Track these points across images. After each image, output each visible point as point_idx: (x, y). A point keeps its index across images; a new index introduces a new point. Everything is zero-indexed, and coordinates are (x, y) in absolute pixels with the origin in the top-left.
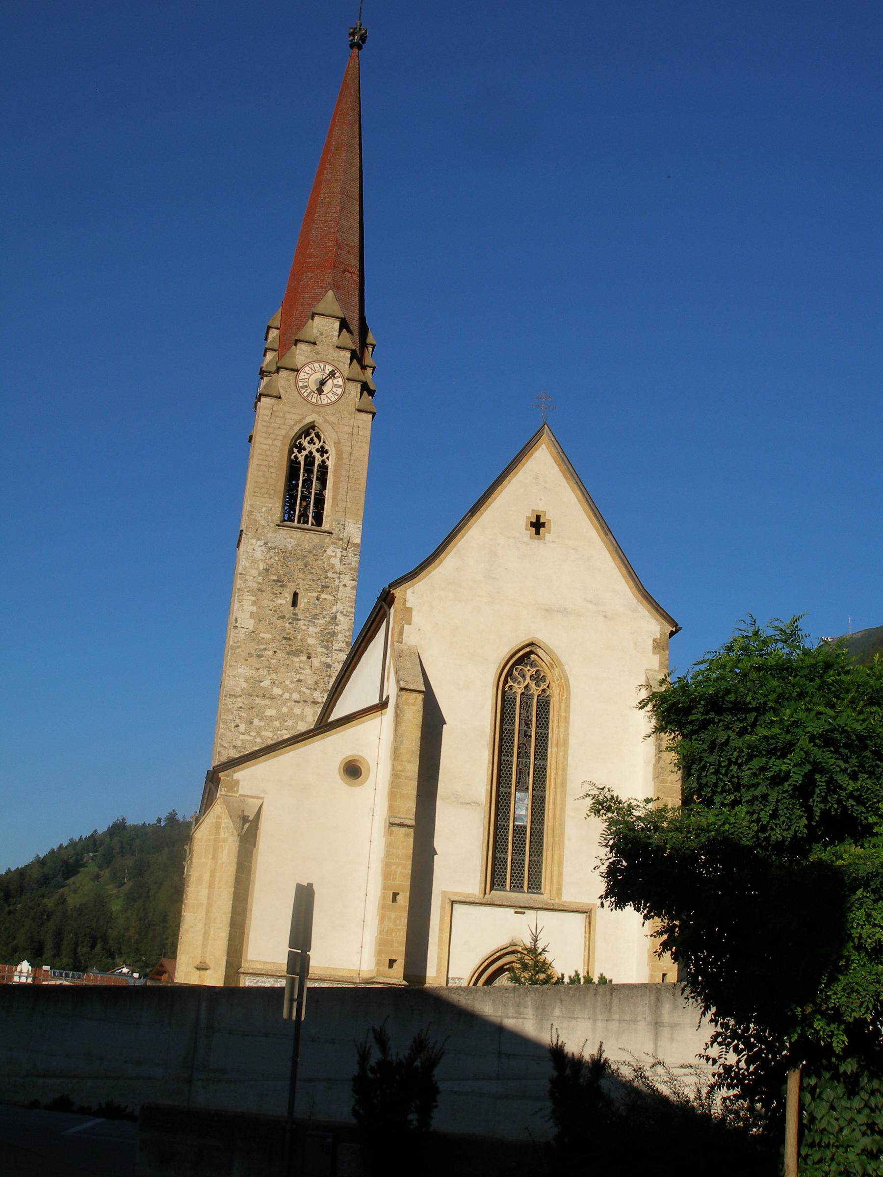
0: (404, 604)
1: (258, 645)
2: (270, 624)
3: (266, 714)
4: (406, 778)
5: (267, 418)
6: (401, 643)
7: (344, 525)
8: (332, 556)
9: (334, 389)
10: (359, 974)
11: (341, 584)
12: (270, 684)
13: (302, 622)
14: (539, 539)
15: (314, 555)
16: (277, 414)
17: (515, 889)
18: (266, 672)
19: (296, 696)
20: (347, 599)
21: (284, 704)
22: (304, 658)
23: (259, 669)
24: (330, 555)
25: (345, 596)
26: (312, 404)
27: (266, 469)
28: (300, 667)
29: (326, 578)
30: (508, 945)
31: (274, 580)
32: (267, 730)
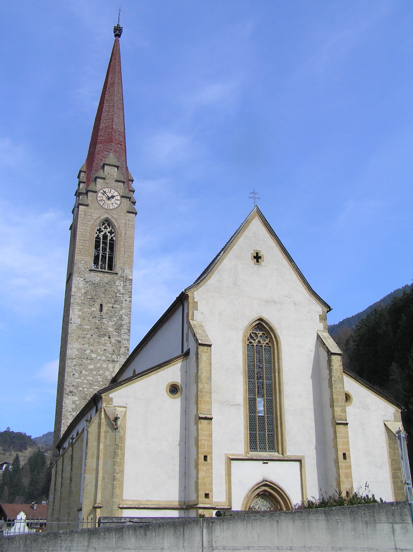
0: (193, 300)
1: (83, 332)
2: (88, 321)
3: (89, 368)
4: (206, 392)
5: (83, 216)
6: (193, 320)
7: (124, 270)
8: (119, 286)
9: (116, 201)
10: (185, 503)
11: (124, 300)
12: (90, 352)
13: (105, 320)
14: (258, 264)
15: (109, 285)
16: (88, 214)
17: (261, 450)
18: (88, 346)
19: (103, 358)
20: (127, 307)
21: (98, 362)
22: (107, 338)
23: (84, 344)
24: (117, 285)
25: (126, 306)
26: (105, 209)
27: (83, 242)
28: (105, 343)
29: (116, 297)
30: (262, 481)
31: (89, 298)
32: (89, 376)
